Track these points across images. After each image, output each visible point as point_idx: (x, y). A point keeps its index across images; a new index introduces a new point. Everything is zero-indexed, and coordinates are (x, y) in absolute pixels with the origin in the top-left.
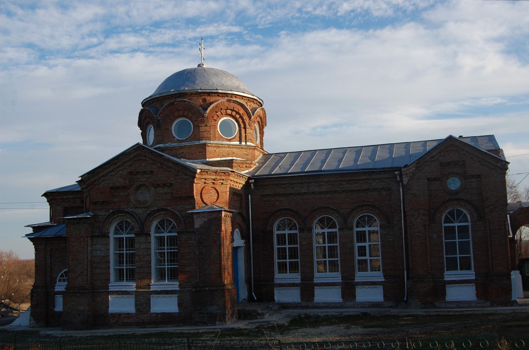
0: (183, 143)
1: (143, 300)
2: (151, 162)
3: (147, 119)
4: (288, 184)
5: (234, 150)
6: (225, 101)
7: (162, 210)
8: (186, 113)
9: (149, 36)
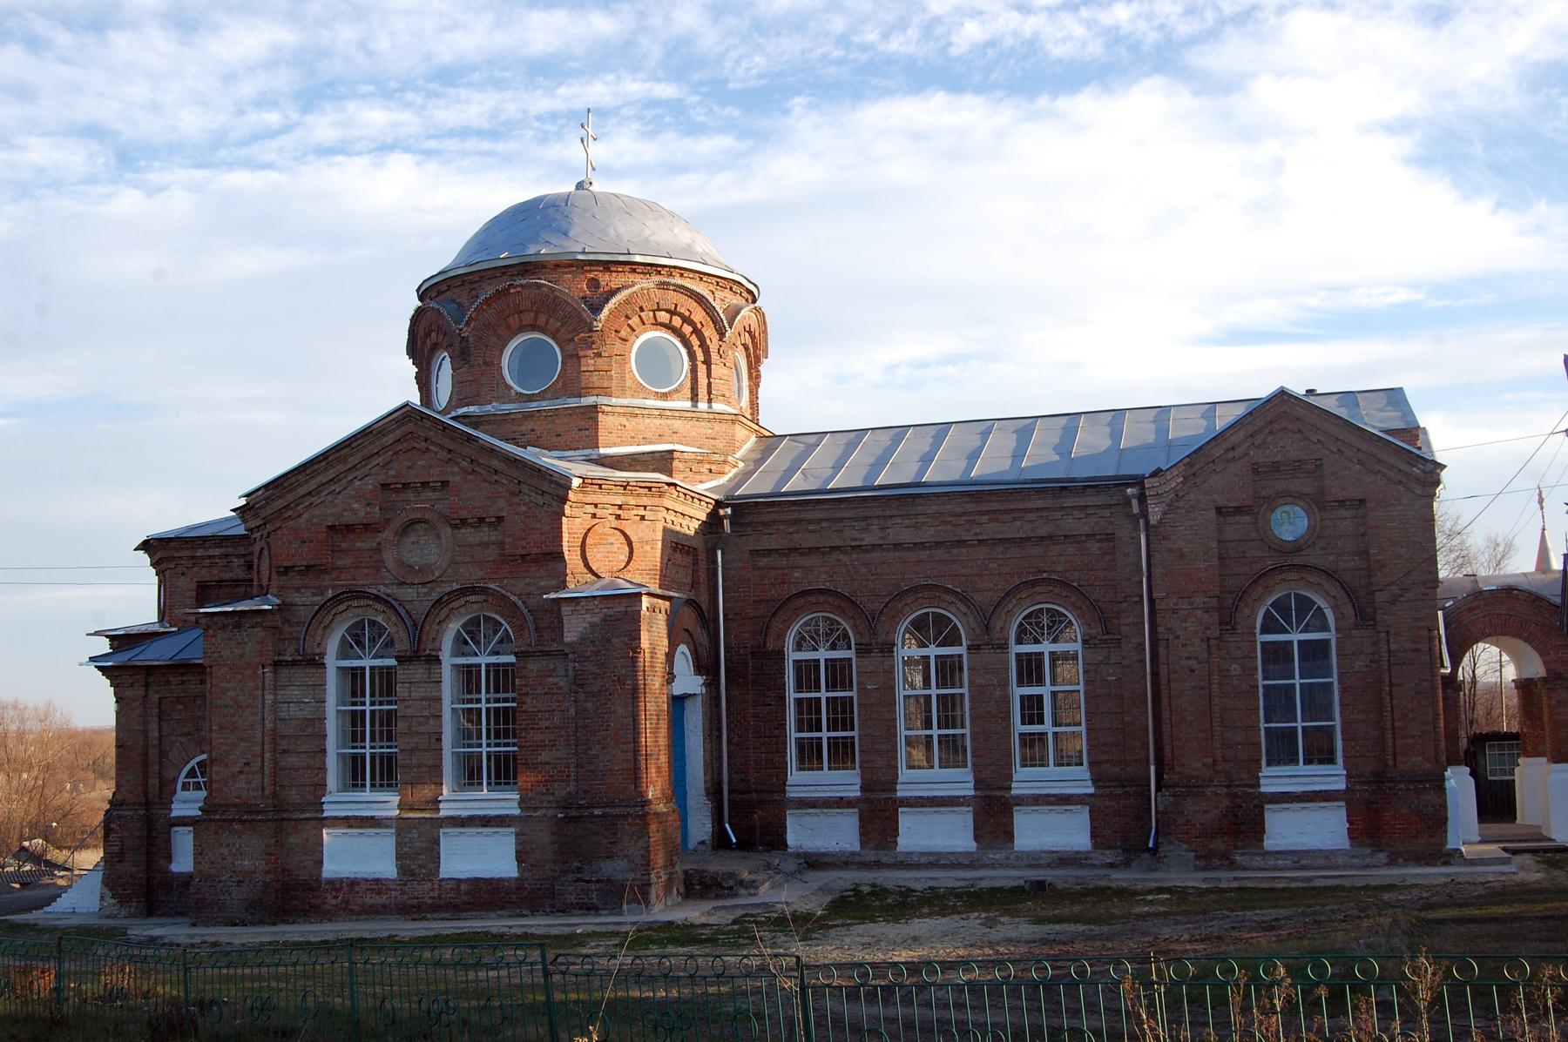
0: (534, 404)
1: (418, 842)
2: (444, 454)
3: (433, 335)
5: (677, 424)
7: (474, 590)
8: (542, 318)
9: (424, 107)
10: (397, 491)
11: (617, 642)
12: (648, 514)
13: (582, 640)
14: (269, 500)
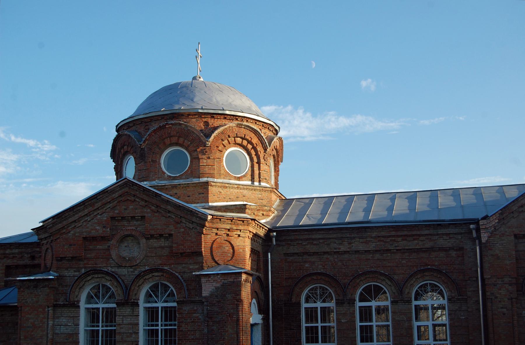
0: (176, 181)
2: (143, 203)
3: (125, 147)
4: (323, 239)
5: (245, 192)
6: (234, 125)
7: (157, 270)
8: (181, 140)
10: (118, 221)
11: (229, 296)
12: (242, 234)
13: (212, 295)
14: (54, 224)
